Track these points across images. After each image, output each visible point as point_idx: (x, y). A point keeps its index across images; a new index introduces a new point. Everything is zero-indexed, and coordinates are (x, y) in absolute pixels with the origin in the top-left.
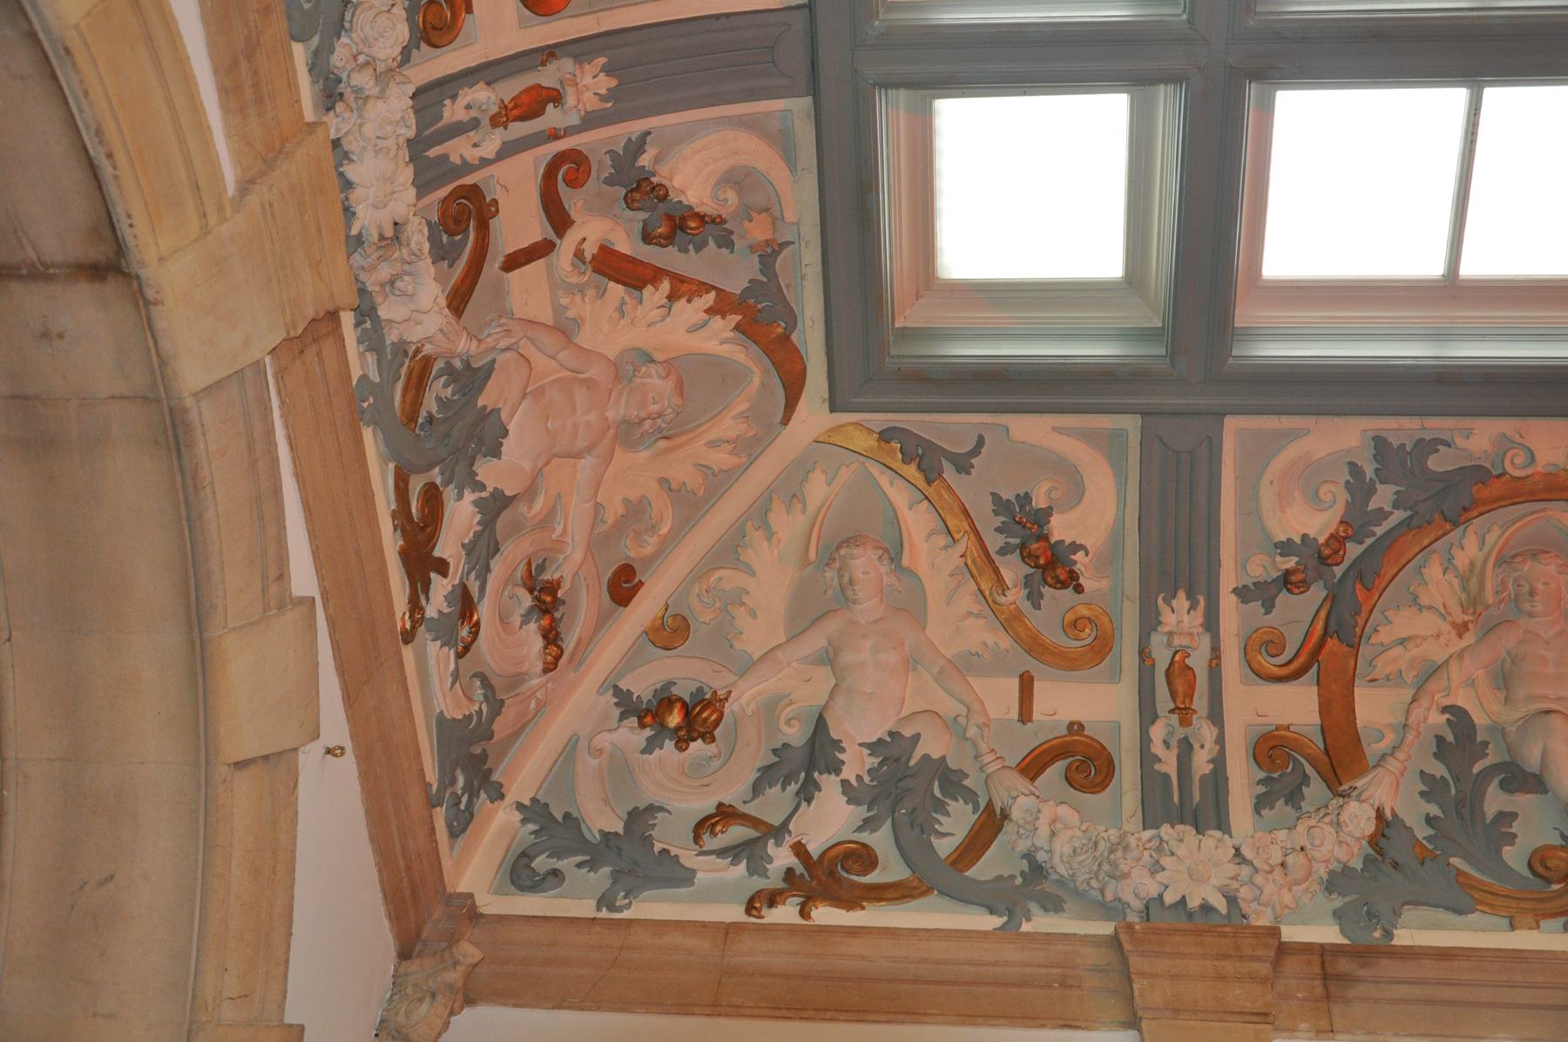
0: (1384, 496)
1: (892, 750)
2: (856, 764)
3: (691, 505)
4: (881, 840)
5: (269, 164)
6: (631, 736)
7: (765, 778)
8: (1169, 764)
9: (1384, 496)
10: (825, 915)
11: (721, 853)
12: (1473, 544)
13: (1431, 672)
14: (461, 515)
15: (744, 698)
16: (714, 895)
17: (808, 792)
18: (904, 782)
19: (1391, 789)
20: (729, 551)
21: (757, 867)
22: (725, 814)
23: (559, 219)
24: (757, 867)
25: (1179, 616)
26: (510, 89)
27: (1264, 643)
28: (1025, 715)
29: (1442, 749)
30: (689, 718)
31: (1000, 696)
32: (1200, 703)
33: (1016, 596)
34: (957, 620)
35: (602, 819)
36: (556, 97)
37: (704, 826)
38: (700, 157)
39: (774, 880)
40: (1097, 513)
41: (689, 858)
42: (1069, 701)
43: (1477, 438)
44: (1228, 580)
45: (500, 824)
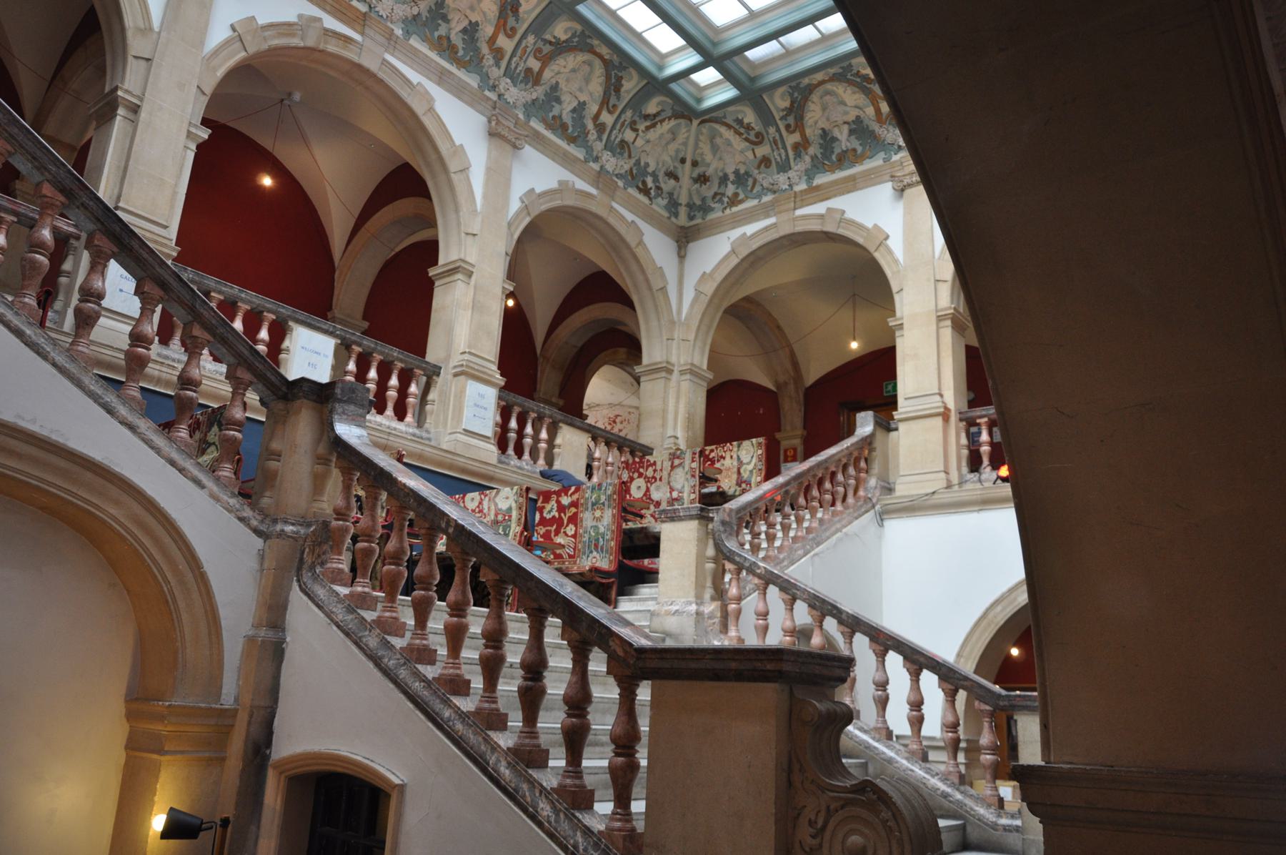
0: (796, 95)
1: (736, 172)
2: (732, 177)
3: (685, 144)
5: (830, 679)
6: (697, 186)
9: (796, 95)
10: (735, 209)
12: (815, 97)
14: (649, 180)
20: (696, 146)
22: (716, 194)
23: (636, 130)
25: (772, 130)
26: (618, 127)
27: (788, 127)
30: (702, 179)
31: (750, 155)
34: (738, 144)
35: (698, 203)
37: (714, 197)
38: (652, 107)
40: (750, 117)
43: (806, 81)
44: (777, 118)
45: (683, 211)
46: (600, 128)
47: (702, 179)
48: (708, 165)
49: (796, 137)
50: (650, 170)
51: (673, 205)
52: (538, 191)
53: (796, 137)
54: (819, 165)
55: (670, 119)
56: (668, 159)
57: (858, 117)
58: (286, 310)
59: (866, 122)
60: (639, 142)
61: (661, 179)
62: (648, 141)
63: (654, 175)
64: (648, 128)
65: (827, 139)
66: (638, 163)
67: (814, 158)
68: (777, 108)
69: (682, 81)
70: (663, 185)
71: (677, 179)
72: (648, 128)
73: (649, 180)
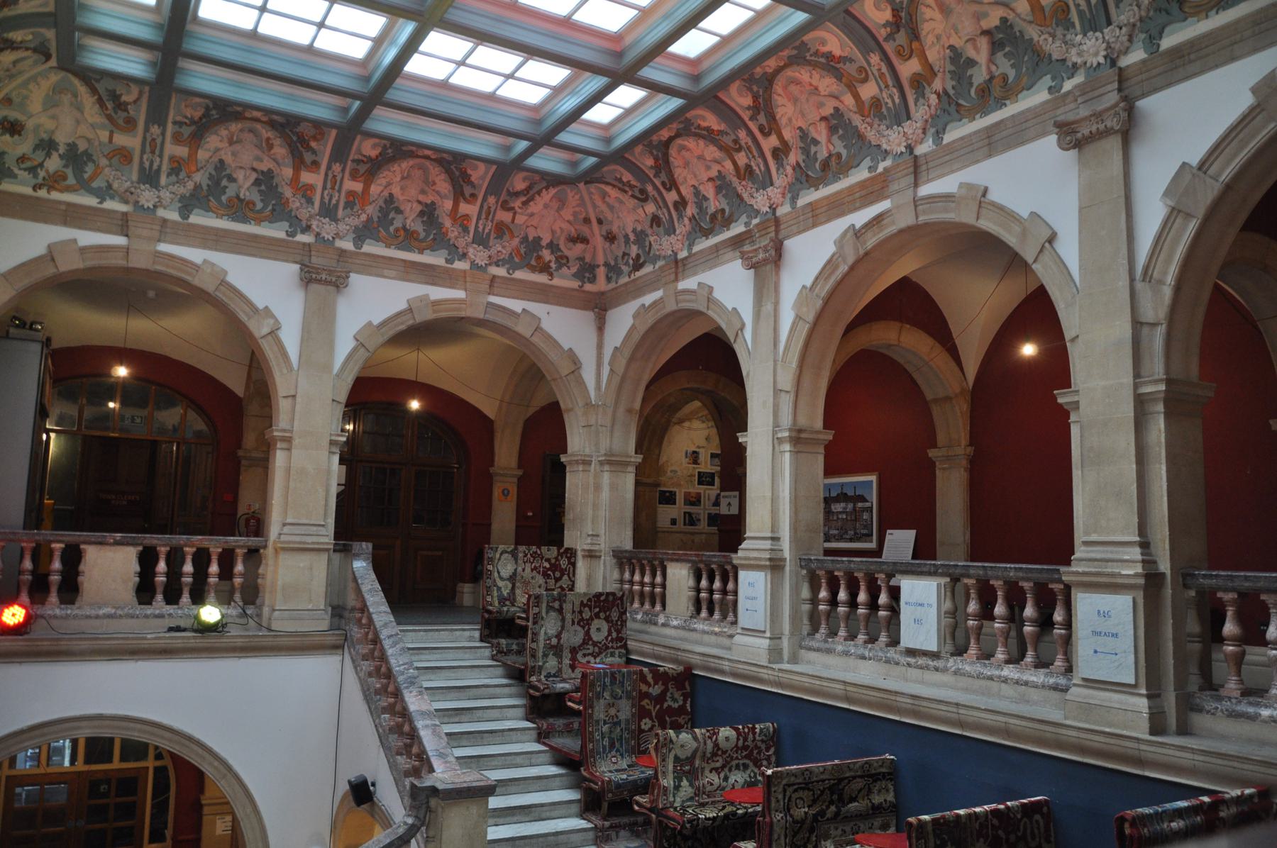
1: (72, 147)
2: (632, 237)
4: (69, 172)
7: (36, 148)
8: (147, 165)
9: (755, 88)
10: (638, 274)
11: (25, 170)
12: (778, 87)
13: (217, 150)
14: (547, 255)
15: (30, 124)
16: (23, 183)
17: (48, 155)
18: (76, 158)
19: (200, 178)
21: (36, 176)
24: (36, 176)
27: (761, 129)
28: (111, 140)
29: (216, 168)
32: (157, 152)
33: (110, 112)
36: (154, 140)
39: (40, 180)
41: (16, 171)
42: (121, 140)
46: (462, 222)
47: (610, 238)
48: (611, 223)
49: (773, 141)
50: (544, 243)
51: (587, 271)
52: (376, 322)
53: (773, 141)
54: (952, 108)
55: (547, 188)
56: (565, 226)
57: (837, 109)
58: (73, 536)
59: (1019, 25)
60: (520, 219)
61: (562, 247)
62: (532, 215)
63: (552, 246)
64: (525, 203)
65: (960, 63)
66: (525, 239)
67: (943, 95)
68: (741, 107)
69: (574, 126)
70: (567, 253)
71: (585, 240)
72: (525, 203)
73: (547, 255)
